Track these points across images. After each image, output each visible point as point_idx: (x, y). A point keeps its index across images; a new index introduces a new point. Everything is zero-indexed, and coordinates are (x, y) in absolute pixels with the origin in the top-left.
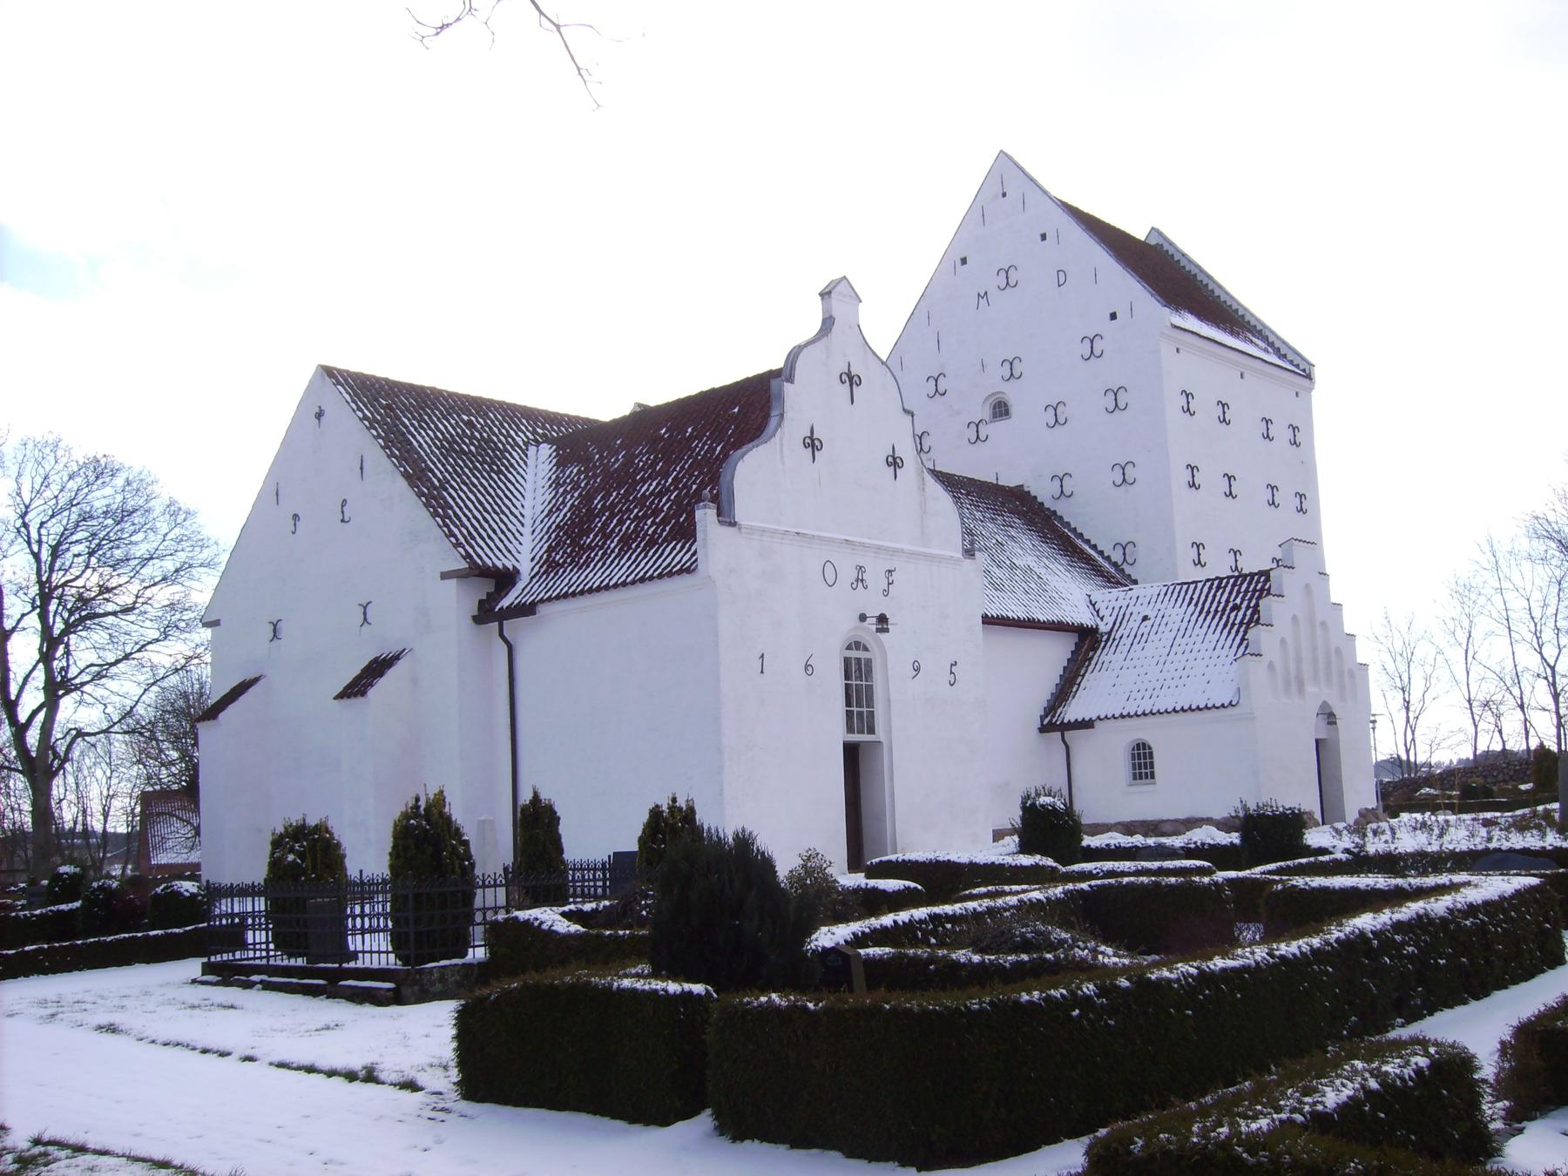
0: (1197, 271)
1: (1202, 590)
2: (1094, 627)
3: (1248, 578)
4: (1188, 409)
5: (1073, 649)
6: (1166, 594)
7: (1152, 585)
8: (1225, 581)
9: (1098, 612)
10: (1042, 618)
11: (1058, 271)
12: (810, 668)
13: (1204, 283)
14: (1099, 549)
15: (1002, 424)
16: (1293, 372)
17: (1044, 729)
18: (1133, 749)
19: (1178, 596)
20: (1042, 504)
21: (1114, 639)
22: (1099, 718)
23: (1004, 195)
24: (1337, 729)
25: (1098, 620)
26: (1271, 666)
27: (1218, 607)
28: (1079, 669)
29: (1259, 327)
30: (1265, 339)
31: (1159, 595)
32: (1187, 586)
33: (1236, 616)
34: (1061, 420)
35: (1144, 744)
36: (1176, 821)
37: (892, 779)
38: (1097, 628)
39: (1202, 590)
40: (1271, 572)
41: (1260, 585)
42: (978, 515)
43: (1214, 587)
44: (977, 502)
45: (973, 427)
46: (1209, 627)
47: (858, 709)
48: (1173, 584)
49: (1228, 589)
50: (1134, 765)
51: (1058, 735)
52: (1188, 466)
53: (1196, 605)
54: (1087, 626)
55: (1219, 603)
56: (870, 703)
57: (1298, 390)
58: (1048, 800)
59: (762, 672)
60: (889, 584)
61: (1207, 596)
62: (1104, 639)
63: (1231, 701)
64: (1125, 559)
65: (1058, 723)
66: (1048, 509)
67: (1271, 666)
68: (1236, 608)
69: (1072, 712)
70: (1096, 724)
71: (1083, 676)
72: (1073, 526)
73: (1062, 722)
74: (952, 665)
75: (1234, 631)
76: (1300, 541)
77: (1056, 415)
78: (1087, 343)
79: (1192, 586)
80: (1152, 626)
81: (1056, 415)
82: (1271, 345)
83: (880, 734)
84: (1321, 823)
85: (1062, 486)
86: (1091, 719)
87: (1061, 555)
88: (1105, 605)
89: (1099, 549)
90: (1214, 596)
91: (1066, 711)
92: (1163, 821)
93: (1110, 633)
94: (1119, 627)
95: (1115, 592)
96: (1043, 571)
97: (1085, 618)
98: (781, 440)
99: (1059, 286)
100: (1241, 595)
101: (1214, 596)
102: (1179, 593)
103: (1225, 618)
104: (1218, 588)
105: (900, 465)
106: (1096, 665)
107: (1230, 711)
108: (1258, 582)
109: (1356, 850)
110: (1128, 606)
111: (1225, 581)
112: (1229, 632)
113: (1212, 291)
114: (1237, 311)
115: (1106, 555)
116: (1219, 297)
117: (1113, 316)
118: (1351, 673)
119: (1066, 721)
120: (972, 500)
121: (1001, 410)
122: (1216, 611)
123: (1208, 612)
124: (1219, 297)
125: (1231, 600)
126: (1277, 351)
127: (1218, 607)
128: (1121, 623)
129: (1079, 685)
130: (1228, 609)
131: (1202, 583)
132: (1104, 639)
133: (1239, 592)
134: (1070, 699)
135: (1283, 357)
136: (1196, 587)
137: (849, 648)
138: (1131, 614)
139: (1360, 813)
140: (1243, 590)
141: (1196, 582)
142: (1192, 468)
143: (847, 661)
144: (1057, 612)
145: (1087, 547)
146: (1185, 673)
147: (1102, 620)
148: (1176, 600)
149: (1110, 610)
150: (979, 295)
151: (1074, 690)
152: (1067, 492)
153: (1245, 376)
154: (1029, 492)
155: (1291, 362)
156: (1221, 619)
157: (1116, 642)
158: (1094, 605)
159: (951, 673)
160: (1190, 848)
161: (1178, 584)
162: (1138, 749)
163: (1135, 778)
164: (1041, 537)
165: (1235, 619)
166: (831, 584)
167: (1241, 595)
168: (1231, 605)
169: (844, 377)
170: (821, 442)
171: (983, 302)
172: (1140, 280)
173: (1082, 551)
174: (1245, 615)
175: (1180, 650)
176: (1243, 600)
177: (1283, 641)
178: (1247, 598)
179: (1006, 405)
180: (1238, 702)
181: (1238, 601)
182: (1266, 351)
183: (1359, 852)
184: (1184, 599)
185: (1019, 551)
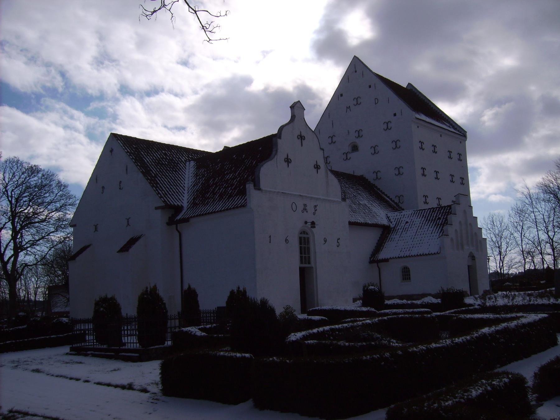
3: (444, 208)
6: (414, 214)
7: (407, 211)
8: (435, 209)
9: (390, 220)
10: (370, 222)
11: (375, 99)
12: (287, 241)
15: (355, 154)
16: (459, 134)
17: (371, 262)
19: (418, 215)
21: (396, 230)
22: (390, 258)
23: (356, 72)
25: (390, 223)
26: (452, 239)
27: (433, 218)
30: (449, 123)
31: (412, 214)
33: (439, 222)
35: (406, 267)
36: (418, 295)
46: (430, 225)
48: (416, 210)
49: (436, 212)
51: (376, 264)
53: (425, 218)
55: (433, 217)
56: (309, 253)
58: (372, 287)
59: (270, 242)
60: (315, 210)
62: (392, 230)
64: (399, 202)
65: (376, 260)
66: (372, 184)
68: (439, 218)
69: (382, 255)
70: (390, 260)
71: (385, 243)
72: (381, 190)
73: (377, 260)
79: (424, 211)
80: (409, 225)
82: (451, 125)
83: (313, 264)
84: (470, 294)
86: (388, 258)
88: (392, 218)
90: (432, 214)
93: (394, 228)
94: (398, 226)
96: (370, 206)
97: (385, 222)
99: (376, 104)
101: (432, 214)
102: (419, 213)
108: (447, 209)
109: (482, 305)
111: (435, 209)
112: (437, 227)
117: (395, 115)
119: (379, 259)
121: (355, 148)
122: (432, 220)
125: (438, 216)
127: (433, 218)
129: (383, 246)
132: (392, 230)
133: (440, 213)
134: (380, 251)
138: (402, 221)
140: (442, 212)
141: (425, 210)
143: (300, 238)
144: (375, 220)
148: (418, 216)
149: (394, 220)
150: (347, 107)
156: (434, 222)
157: (396, 231)
158: (388, 218)
159: (338, 242)
163: (403, 280)
168: (437, 217)
169: (299, 137)
171: (348, 110)
174: (442, 221)
175: (419, 234)
176: (442, 216)
177: (456, 230)
179: (357, 146)
181: (440, 216)
182: (449, 127)
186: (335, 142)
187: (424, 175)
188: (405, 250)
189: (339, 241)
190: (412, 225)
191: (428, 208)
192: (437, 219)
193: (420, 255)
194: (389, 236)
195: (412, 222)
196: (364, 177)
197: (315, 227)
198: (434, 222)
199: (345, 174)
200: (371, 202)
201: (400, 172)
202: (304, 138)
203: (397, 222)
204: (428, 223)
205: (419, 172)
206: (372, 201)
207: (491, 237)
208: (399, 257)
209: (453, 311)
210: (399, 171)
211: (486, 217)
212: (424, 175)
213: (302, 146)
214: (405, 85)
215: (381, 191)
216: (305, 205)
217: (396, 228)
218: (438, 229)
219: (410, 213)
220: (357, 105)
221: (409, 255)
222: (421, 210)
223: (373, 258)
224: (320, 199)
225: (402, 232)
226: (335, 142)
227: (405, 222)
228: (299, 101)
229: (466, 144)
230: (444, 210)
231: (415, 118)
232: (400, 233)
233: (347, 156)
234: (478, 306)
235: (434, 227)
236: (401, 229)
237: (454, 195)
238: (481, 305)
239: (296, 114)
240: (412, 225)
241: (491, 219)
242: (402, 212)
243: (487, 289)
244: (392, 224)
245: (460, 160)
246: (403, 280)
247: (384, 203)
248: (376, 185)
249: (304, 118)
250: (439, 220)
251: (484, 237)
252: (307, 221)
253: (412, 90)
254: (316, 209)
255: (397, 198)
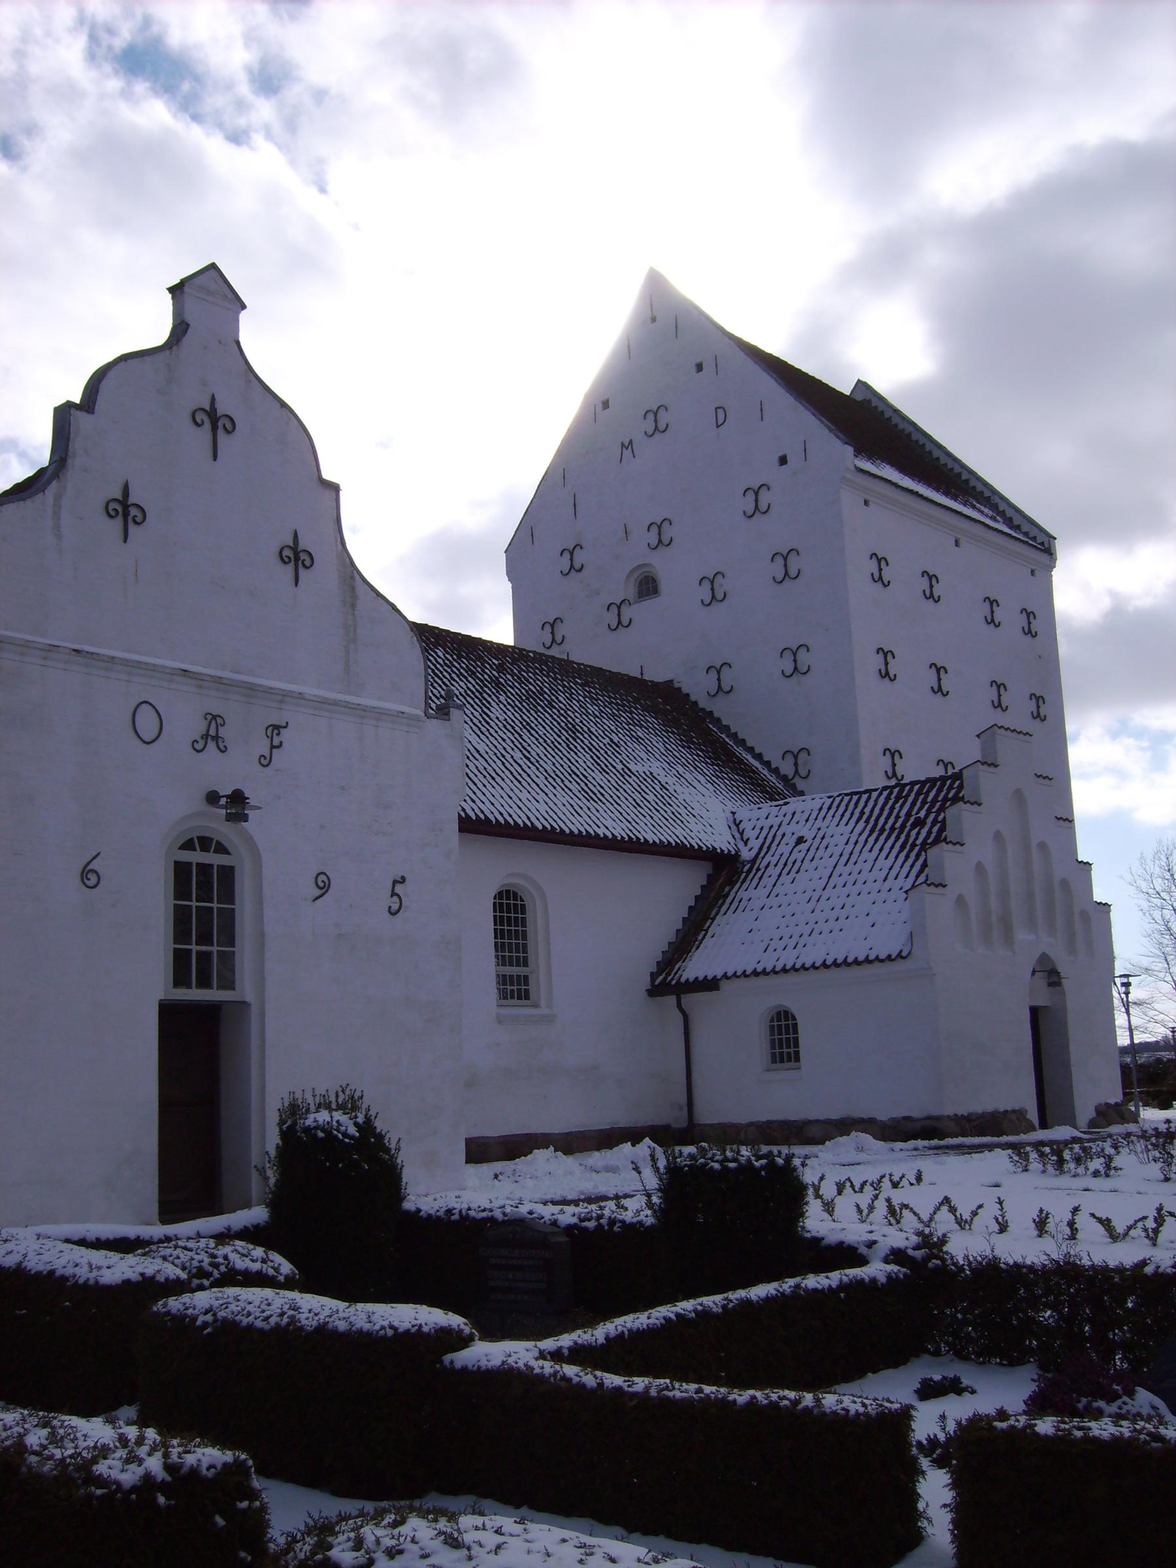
0: (911, 429)
1: (876, 801)
2: (733, 853)
3: (938, 783)
4: (881, 578)
5: (705, 883)
6: (829, 808)
7: (813, 796)
8: (907, 788)
9: (742, 834)
10: (651, 837)
13: (921, 443)
14: (766, 759)
15: (649, 604)
16: (1027, 543)
17: (656, 990)
18: (772, 1020)
19: (845, 811)
20: (696, 703)
21: (758, 869)
22: (725, 976)
24: (1063, 993)
25: (741, 845)
26: (960, 901)
27: (895, 822)
28: (710, 909)
29: (987, 493)
30: (994, 507)
31: (820, 809)
32: (849, 797)
33: (918, 834)
34: (720, 596)
35: (786, 1012)
36: (828, 1122)
37: (262, 1066)
38: (737, 855)
39: (876, 801)
40: (964, 771)
41: (953, 792)
42: (592, 709)
43: (893, 796)
44: (597, 694)
45: (614, 609)
46: (881, 850)
47: (200, 948)
48: (840, 795)
49: (910, 799)
50: (773, 1041)
51: (671, 1000)
52: (879, 650)
53: (867, 821)
54: (722, 851)
55: (898, 817)
56: (229, 938)
57: (1033, 567)
58: (323, 1116)
60: (273, 747)
61: (882, 810)
62: (745, 869)
63: (901, 951)
64: (796, 772)
65: (674, 982)
66: (703, 710)
67: (960, 901)
68: (920, 823)
69: (695, 967)
71: (713, 919)
72: (733, 731)
74: (395, 882)
75: (883, 838)
76: (1008, 729)
77: (712, 589)
78: (751, 496)
79: (865, 797)
80: (808, 850)
81: (712, 589)
82: (1002, 514)
83: (246, 990)
84: (1036, 1122)
85: (719, 680)
87: (706, 763)
88: (751, 824)
89: (766, 759)
90: (892, 808)
91: (686, 967)
92: (810, 1122)
93: (754, 861)
94: (766, 853)
95: (767, 807)
96: (671, 780)
97: (721, 839)
98: (58, 499)
99: (718, 426)
100: (927, 806)
101: (892, 808)
102: (847, 806)
103: (903, 837)
104: (898, 798)
105: (308, 563)
106: (731, 904)
107: (899, 966)
108: (951, 788)
109: (918, 1254)
110: (780, 826)
111: (907, 788)
112: (907, 857)
113: (930, 452)
114: (959, 475)
115: (773, 766)
116: (938, 459)
117: (783, 460)
118: (1085, 915)
119: (683, 980)
120: (589, 692)
121: (648, 586)
122: (893, 829)
123: (882, 830)
124: (938, 459)
125: (914, 813)
126: (1009, 522)
127: (895, 822)
128: (769, 848)
129: (707, 931)
130: (909, 824)
131: (878, 792)
132: (745, 869)
133: (924, 802)
135: (1017, 528)
136: (869, 798)
137: (188, 845)
138: (784, 835)
139: (1097, 1109)
140: (929, 799)
141: (869, 791)
142: (886, 654)
143: (181, 871)
144: (679, 831)
145: (749, 757)
146: (843, 913)
147: (746, 844)
148: (842, 816)
149: (757, 831)
150: (623, 445)
151: (700, 938)
152: (726, 688)
153: (962, 542)
154: (680, 688)
155: (1026, 534)
156: (897, 838)
157: (760, 873)
158: (737, 826)
159: (393, 894)
160: (586, 1229)
161: (847, 795)
162: (779, 1020)
163: (774, 1061)
164: (681, 740)
165: (916, 839)
166: (147, 738)
167: (927, 806)
168: (912, 819)
169: (200, 417)
170: (143, 511)
171: (627, 453)
172: (816, 413)
173: (741, 761)
174: (929, 832)
175: (842, 881)
176: (929, 812)
177: (980, 867)
178: (934, 810)
179: (654, 580)
180: (910, 953)
181: (922, 814)
182: (993, 519)
183: (928, 1258)
184: (852, 814)
185: (644, 756)
186: (582, 566)
187: (885, 675)
188: (782, 943)
189: (399, 889)
190: (817, 849)
191: (880, 787)
192: (909, 824)
193: (835, 964)
194: (732, 894)
195: (818, 840)
196: (676, 685)
197: (245, 818)
198: (897, 838)
199: (597, 672)
200: (681, 770)
201: (798, 666)
202: (229, 426)
203: (765, 838)
204: (876, 840)
205: (868, 664)
206: (683, 765)
207: (1163, 920)
208: (755, 973)
209: (566, 1340)
210: (795, 661)
211: (1149, 855)
212: (885, 675)
213: (215, 457)
214: (845, 387)
215: (734, 736)
216: (214, 717)
217: (758, 861)
218: (910, 861)
219: (817, 804)
220: (657, 433)
221: (794, 965)
222: (856, 793)
223: (664, 975)
224: (301, 696)
225: (780, 875)
226: (582, 566)
227: (795, 837)
228: (213, 267)
229: (1054, 578)
230: (940, 791)
231: (854, 469)
232: (774, 878)
233: (619, 615)
234: (886, 1261)
235: (897, 857)
236: (776, 865)
237: (977, 734)
238: (910, 1252)
239: (188, 317)
240: (817, 849)
241: (1165, 860)
242: (786, 804)
243: (1112, 1101)
244: (749, 847)
245: (1029, 632)
246: (774, 1061)
247: (738, 774)
248: (716, 715)
249: (238, 343)
250: (916, 830)
251: (1099, 895)
252: (215, 792)
253: (870, 401)
254: (276, 742)
255: (789, 758)
